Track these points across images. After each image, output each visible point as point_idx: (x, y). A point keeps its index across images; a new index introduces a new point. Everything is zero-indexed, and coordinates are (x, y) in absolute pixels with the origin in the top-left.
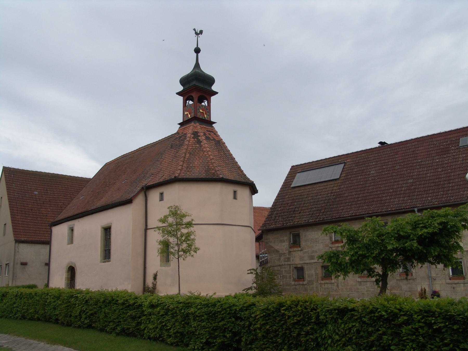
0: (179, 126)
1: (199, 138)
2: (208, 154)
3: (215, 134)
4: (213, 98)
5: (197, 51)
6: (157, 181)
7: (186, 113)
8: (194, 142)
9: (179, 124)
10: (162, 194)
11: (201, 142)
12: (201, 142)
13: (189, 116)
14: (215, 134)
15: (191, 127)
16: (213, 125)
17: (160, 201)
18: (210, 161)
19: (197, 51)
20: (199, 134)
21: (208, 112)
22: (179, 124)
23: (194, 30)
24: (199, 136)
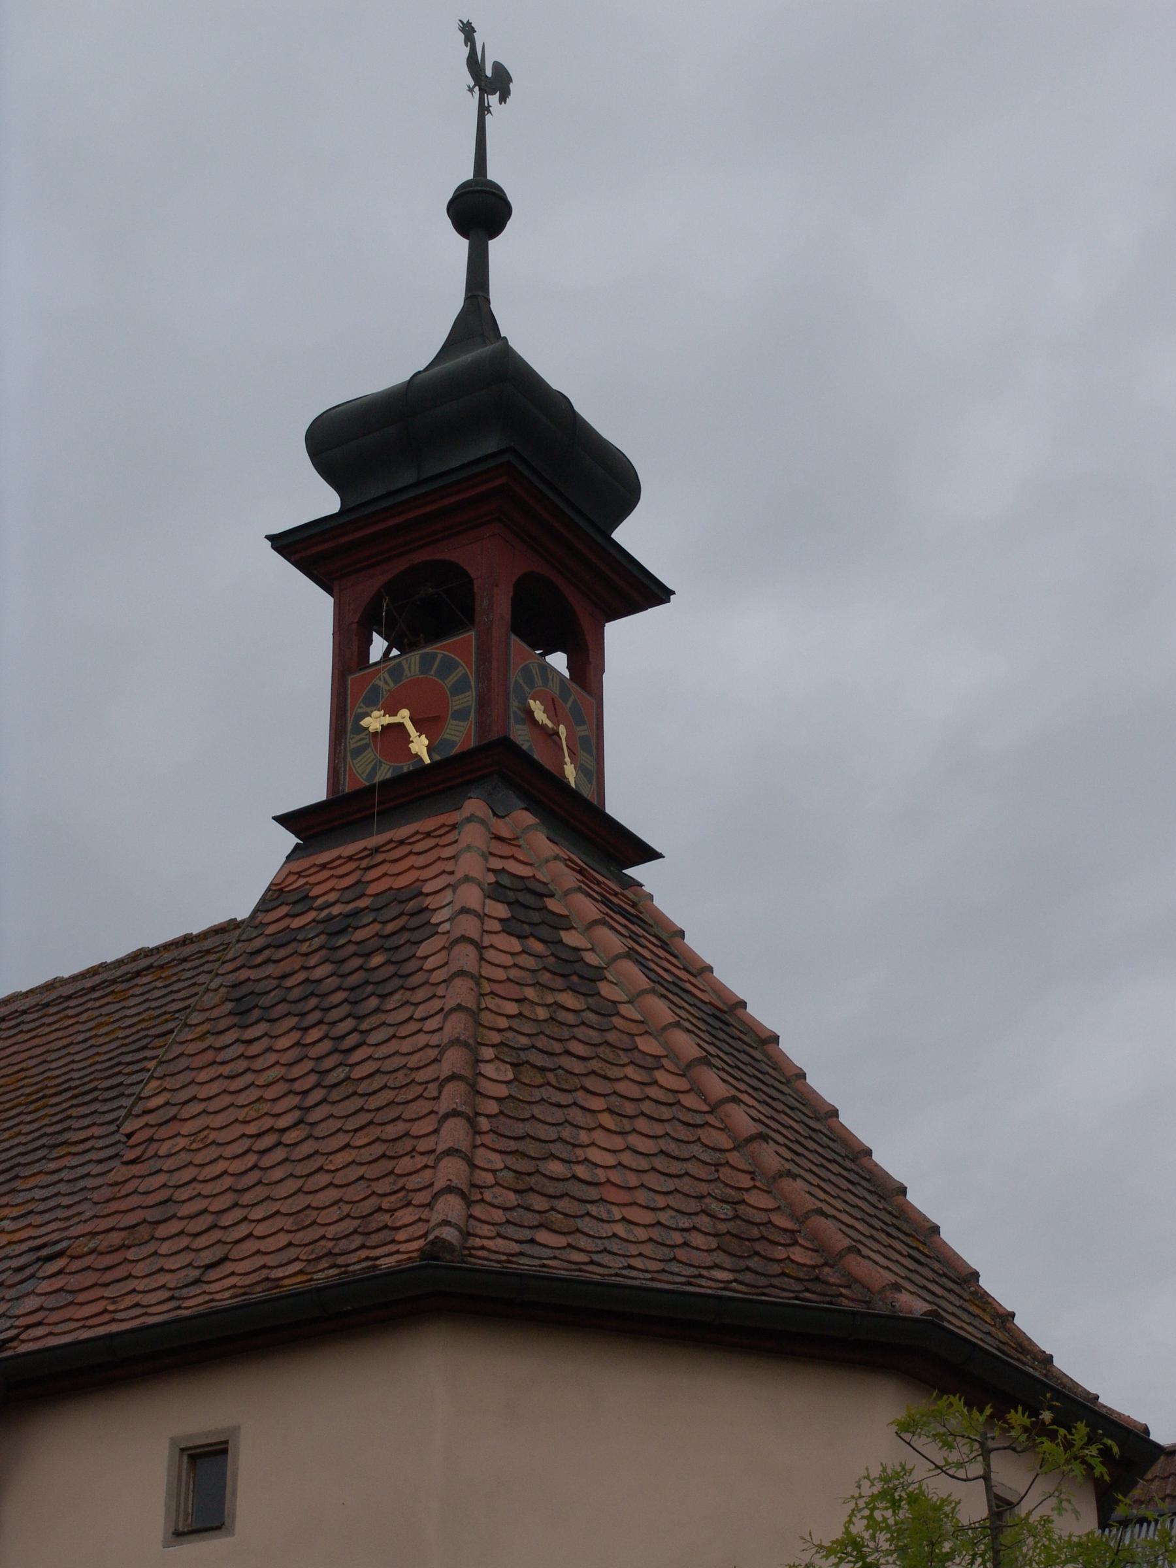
0: (290, 840)
1: (571, 938)
2: (697, 1090)
3: (664, 946)
4: (620, 635)
5: (479, 211)
6: (147, 1297)
7: (375, 721)
8: (529, 962)
9: (287, 820)
10: (205, 1469)
11: (595, 975)
12: (595, 975)
13: (419, 745)
14: (664, 946)
15: (472, 835)
16: (634, 872)
17: (178, 1535)
18: (734, 1158)
19: (479, 211)
20: (552, 905)
21: (585, 741)
22: (287, 820)
23: (468, 30)
24: (563, 923)
